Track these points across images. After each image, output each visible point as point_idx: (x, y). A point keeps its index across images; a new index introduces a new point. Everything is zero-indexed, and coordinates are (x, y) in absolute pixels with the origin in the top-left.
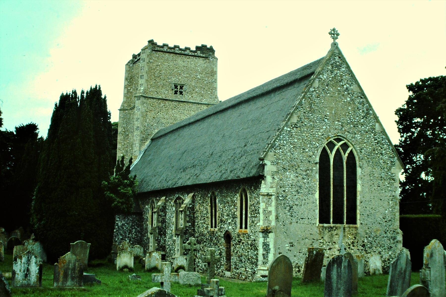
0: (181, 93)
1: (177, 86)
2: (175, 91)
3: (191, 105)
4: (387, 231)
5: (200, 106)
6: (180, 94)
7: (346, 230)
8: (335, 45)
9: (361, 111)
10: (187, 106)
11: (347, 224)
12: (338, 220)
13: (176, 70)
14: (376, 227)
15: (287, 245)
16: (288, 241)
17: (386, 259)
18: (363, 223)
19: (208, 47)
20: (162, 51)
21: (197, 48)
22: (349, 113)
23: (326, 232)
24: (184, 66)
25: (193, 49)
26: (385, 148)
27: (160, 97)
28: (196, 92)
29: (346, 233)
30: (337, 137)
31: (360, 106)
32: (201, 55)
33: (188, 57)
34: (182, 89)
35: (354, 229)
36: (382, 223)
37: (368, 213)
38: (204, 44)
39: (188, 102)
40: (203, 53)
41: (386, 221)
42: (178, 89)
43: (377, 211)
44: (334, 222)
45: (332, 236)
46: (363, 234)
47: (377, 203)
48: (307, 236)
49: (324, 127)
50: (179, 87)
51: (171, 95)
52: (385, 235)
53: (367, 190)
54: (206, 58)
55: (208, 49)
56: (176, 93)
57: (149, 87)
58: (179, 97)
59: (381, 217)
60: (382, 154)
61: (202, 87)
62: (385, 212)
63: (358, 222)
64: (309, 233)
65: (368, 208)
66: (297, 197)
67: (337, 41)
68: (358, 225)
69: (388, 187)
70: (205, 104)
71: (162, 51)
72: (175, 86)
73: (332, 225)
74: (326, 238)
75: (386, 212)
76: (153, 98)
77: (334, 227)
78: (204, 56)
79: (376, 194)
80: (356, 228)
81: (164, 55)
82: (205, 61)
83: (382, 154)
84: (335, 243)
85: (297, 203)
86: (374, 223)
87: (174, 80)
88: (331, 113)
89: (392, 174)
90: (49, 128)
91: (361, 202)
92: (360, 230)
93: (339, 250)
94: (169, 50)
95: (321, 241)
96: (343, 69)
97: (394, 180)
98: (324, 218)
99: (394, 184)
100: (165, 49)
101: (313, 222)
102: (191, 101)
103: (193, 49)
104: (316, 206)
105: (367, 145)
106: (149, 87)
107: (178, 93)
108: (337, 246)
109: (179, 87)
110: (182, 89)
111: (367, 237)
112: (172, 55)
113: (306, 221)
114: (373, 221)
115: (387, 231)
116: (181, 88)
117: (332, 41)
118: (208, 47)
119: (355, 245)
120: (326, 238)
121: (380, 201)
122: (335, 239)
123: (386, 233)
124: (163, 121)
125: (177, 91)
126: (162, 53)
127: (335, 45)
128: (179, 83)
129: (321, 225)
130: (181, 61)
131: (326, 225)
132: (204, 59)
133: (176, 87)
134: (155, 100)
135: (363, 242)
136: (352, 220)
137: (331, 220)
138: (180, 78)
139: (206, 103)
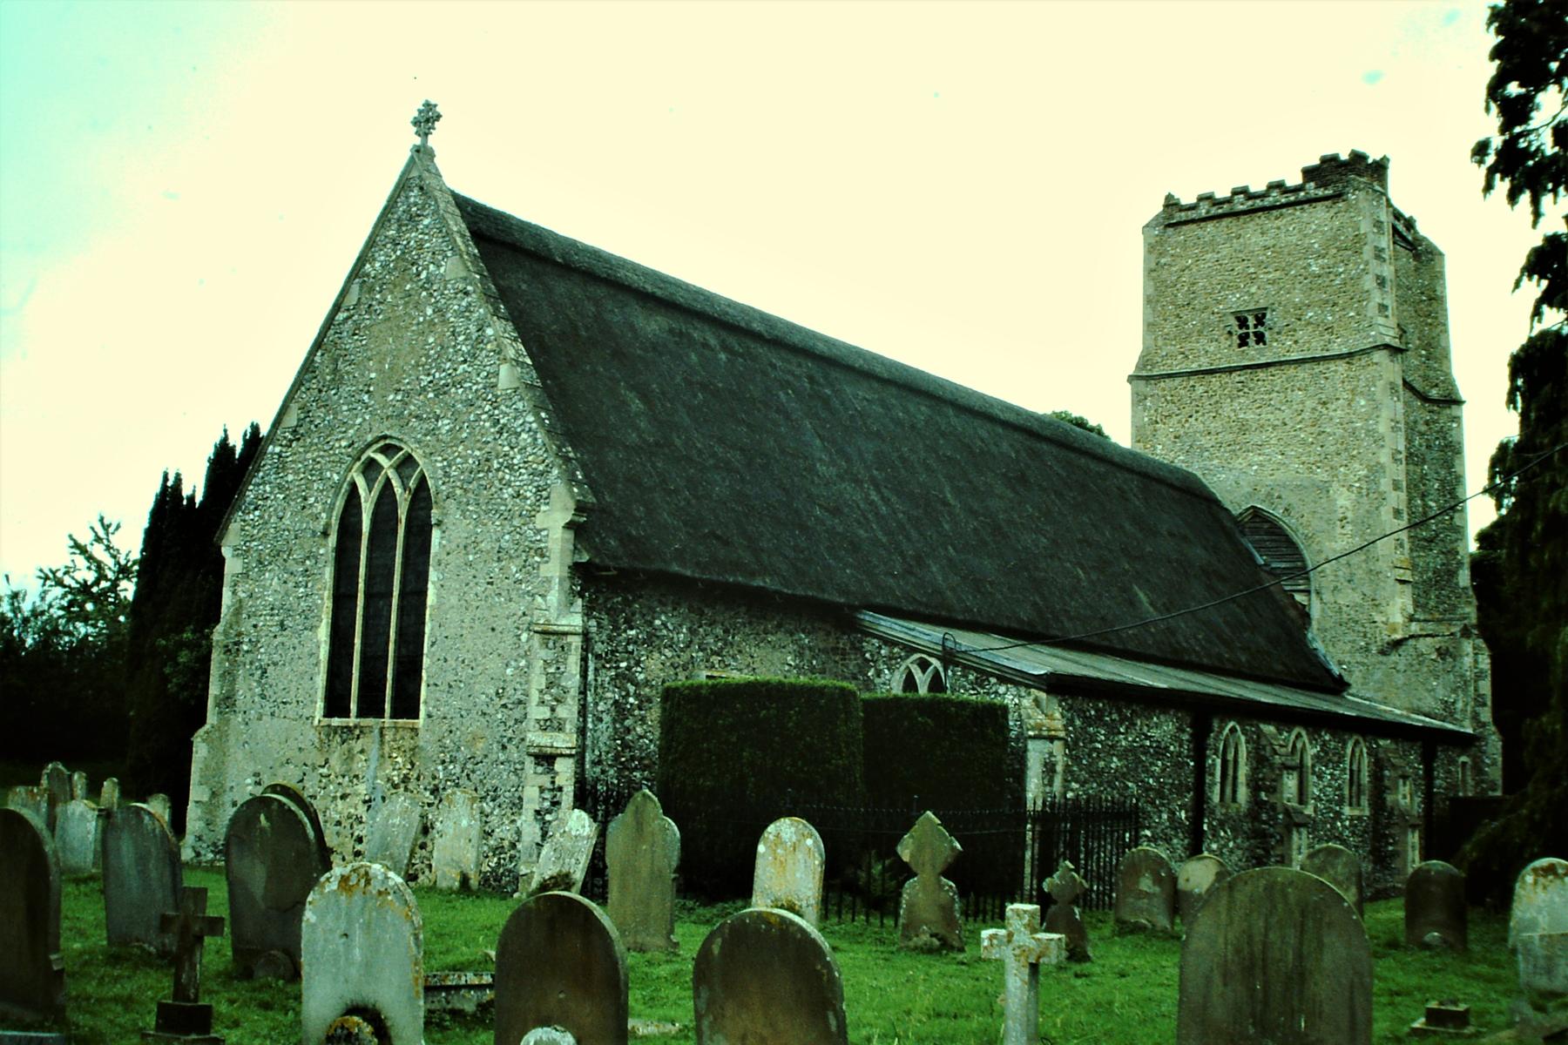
0: (1260, 338)
1: (1246, 320)
2: (1240, 337)
3: (1291, 371)
4: (510, 739)
5: (1321, 367)
6: (1257, 343)
7: (387, 738)
8: (422, 154)
9: (461, 338)
10: (1278, 377)
11: (392, 717)
12: (371, 707)
13: (1239, 268)
14: (475, 725)
15: (249, 781)
16: (251, 769)
17: (506, 843)
18: (434, 712)
19: (1344, 156)
20: (1193, 221)
21: (1309, 173)
22: (428, 356)
23: (334, 744)
24: (1267, 248)
25: (1294, 179)
26: (522, 444)
27: (1194, 367)
28: (1309, 323)
29: (387, 749)
30: (382, 443)
31: (460, 323)
32: (1320, 192)
33: (1275, 213)
34: (1262, 324)
35: (408, 735)
36: (491, 710)
37: (451, 677)
38: (1329, 152)
39: (1281, 363)
40: (1325, 186)
41: (504, 706)
42: (1251, 326)
43: (480, 669)
44: (360, 715)
45: (349, 757)
46: (432, 749)
47: (479, 642)
48: (288, 755)
49: (359, 420)
50: (1251, 322)
51: (1227, 354)
52: (502, 757)
53: (454, 600)
54: (1337, 197)
55: (1345, 164)
56: (1243, 341)
57: (1160, 343)
58: (1254, 354)
59: (492, 691)
60: (510, 467)
61: (1327, 302)
62: (504, 674)
63: (422, 714)
64: (295, 745)
65: (451, 662)
66: (279, 639)
67: (418, 141)
68: (421, 722)
69: (520, 582)
70: (1340, 357)
71: (1193, 221)
72: (1238, 319)
73: (352, 721)
74: (335, 761)
75: (509, 671)
76: (1170, 376)
77: (356, 727)
78: (1329, 192)
79: (478, 613)
80: (414, 730)
81: (1199, 232)
82: (1333, 211)
83: (510, 467)
84: (356, 776)
85: (276, 658)
86: (469, 711)
87: (1236, 301)
88: (380, 371)
89: (539, 531)
90: (146, 525)
91: (433, 644)
92: (424, 738)
93: (365, 802)
94: (1214, 211)
95: (324, 771)
96: (426, 222)
97: (542, 556)
98: (335, 704)
99: (542, 567)
100: (1241, 204)
101: (306, 713)
102: (1294, 356)
103: (1294, 179)
104: (317, 664)
105: (466, 449)
106: (1160, 343)
107: (1252, 339)
108: (362, 788)
109: (1251, 322)
110: (1262, 324)
111: (443, 762)
112: (1225, 222)
113: (291, 710)
114: (465, 706)
115: (510, 739)
116: (1260, 320)
117: (432, 141)
118: (1344, 156)
119: (410, 787)
120: (335, 761)
121: (490, 633)
122: (359, 765)
123: (504, 747)
124: (1205, 441)
125: (1247, 335)
126: (1194, 226)
127: (422, 154)
128: (1251, 307)
129: (326, 721)
130: (1253, 234)
131: (336, 721)
132: (1328, 203)
133: (1243, 322)
134: (1178, 380)
135: (434, 778)
136: (407, 706)
137: (353, 707)
138: (1253, 290)
139: (1345, 351)
